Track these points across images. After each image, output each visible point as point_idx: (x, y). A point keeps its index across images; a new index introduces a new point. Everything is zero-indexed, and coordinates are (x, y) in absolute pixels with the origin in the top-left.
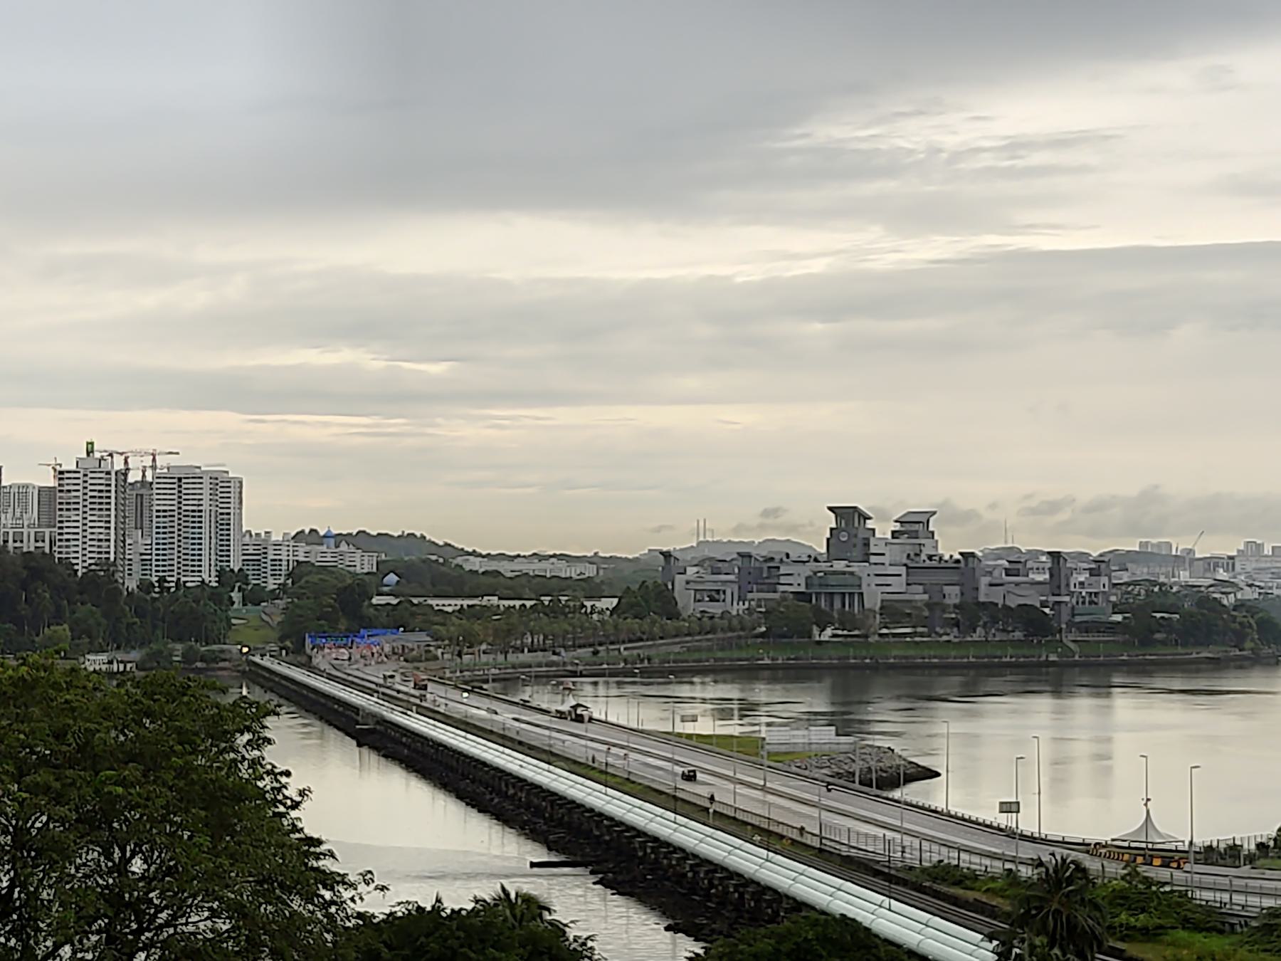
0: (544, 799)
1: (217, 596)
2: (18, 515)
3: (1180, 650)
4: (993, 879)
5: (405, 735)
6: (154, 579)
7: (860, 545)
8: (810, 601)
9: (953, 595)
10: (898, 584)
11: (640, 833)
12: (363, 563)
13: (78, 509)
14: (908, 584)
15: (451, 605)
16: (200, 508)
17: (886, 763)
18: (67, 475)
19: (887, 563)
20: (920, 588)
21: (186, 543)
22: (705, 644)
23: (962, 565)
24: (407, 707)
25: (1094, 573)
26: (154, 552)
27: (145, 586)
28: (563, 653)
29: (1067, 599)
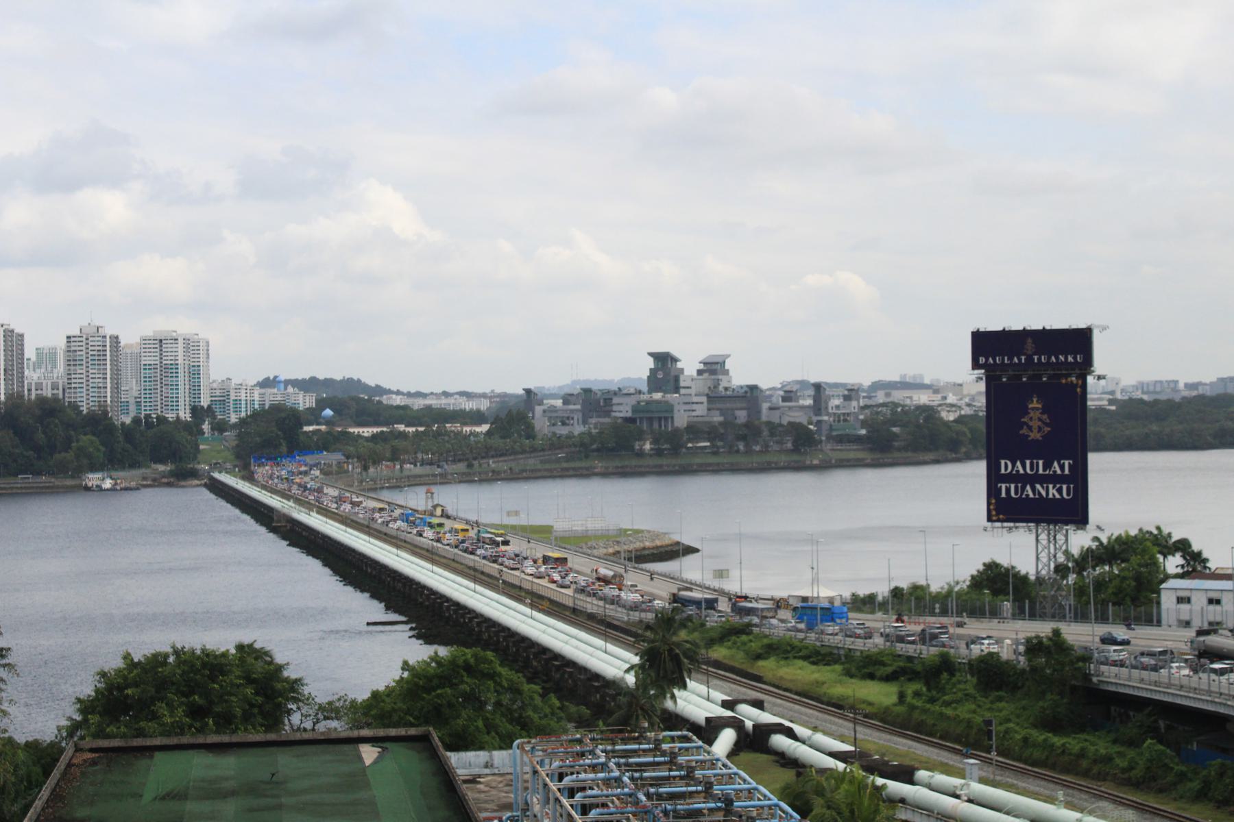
0: (389, 576)
1: (193, 428)
2: (49, 369)
3: (909, 454)
5: (304, 530)
6: (142, 416)
9: (742, 416)
10: (701, 410)
11: (448, 599)
12: (304, 401)
13: (82, 365)
14: (709, 409)
15: (367, 432)
16: (177, 362)
17: (658, 543)
18: (73, 339)
19: (693, 394)
24: (309, 506)
25: (847, 398)
27: (136, 421)
29: (826, 418)
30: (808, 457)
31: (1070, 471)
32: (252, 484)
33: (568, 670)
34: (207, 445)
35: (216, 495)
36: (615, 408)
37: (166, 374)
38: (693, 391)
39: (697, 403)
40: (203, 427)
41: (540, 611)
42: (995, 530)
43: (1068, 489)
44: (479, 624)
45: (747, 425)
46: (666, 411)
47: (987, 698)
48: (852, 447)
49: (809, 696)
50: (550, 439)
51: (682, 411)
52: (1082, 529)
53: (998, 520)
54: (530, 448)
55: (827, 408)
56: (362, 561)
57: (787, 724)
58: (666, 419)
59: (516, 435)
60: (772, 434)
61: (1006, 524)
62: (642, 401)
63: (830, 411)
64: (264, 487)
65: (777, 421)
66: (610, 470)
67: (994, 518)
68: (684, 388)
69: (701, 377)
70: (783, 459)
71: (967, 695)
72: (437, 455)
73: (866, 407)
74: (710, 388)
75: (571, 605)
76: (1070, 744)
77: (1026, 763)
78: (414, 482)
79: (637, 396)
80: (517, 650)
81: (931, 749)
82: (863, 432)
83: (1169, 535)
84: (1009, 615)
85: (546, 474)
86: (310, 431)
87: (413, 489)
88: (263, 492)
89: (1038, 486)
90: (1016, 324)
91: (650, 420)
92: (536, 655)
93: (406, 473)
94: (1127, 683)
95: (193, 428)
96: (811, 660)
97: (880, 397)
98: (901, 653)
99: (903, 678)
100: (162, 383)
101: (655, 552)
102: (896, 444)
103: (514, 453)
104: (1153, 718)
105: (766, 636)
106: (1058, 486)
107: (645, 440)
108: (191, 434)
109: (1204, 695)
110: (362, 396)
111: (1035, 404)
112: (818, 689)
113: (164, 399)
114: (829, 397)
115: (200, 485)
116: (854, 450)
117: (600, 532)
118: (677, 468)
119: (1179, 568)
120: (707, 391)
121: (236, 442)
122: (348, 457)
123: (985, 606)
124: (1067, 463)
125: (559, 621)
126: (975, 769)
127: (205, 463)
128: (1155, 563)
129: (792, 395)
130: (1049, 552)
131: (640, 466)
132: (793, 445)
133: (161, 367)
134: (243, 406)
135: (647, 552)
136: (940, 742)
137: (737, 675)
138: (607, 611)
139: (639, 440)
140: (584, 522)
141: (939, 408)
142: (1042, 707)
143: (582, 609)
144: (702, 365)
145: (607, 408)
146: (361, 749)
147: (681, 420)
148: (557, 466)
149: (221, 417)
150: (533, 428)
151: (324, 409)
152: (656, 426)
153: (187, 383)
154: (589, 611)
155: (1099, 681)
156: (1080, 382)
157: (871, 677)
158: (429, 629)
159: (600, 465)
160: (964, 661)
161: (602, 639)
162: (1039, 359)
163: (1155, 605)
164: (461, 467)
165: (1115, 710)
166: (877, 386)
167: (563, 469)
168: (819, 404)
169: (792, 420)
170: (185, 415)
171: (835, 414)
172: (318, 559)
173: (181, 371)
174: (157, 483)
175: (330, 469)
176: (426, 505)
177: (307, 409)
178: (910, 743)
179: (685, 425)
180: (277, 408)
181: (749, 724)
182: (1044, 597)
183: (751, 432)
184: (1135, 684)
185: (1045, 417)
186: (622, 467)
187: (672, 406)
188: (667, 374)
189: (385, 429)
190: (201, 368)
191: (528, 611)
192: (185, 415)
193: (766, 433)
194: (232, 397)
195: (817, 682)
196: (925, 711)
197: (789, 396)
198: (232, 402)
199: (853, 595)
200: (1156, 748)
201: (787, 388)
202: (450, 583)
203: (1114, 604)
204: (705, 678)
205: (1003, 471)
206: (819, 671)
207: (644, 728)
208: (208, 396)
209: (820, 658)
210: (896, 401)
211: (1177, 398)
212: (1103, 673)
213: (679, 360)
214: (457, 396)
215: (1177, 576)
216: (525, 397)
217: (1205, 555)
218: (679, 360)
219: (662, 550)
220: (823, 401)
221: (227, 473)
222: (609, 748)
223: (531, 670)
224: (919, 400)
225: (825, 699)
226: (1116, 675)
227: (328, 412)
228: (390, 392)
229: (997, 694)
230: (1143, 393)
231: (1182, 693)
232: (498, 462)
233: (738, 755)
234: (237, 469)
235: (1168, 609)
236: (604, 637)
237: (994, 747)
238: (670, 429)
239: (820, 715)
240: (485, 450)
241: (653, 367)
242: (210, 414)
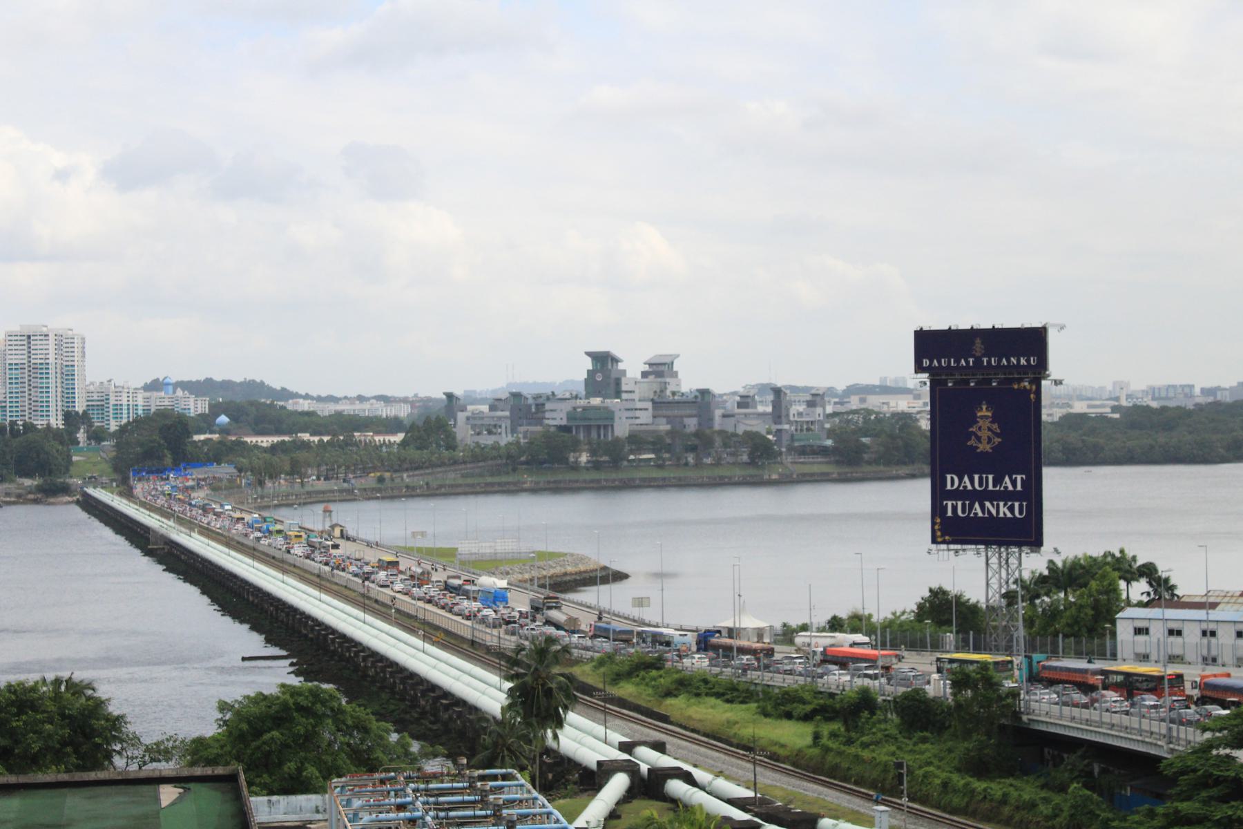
0: (271, 604)
1: (66, 437)
3: (882, 468)
5: (183, 553)
6: (7, 423)
7: (613, 386)
8: (571, 432)
9: (692, 424)
10: (645, 417)
12: (195, 406)
14: (654, 417)
15: (266, 441)
16: (47, 361)
17: (582, 568)
19: (637, 399)
21: (36, 392)
22: (477, 471)
23: (699, 400)
25: (811, 404)
26: (8, 400)
28: (353, 481)
29: (786, 427)
30: (766, 472)
31: (1022, 486)
32: (130, 501)
33: (457, 709)
34: (81, 456)
35: (89, 513)
36: (547, 415)
37: (35, 375)
38: (636, 396)
39: (641, 409)
40: (78, 435)
41: (433, 643)
42: (941, 553)
43: (1021, 507)
44: (365, 659)
45: (697, 434)
46: (607, 417)
47: (910, 739)
48: (816, 460)
49: (718, 738)
50: (472, 451)
51: (624, 419)
52: (1036, 552)
53: (944, 542)
54: (449, 460)
55: (788, 415)
56: (244, 589)
57: (686, 767)
58: (606, 427)
59: (434, 445)
60: (725, 445)
61: (952, 546)
62: (579, 407)
63: (792, 418)
64: (143, 505)
65: (730, 429)
66: (541, 485)
67: (939, 540)
68: (626, 392)
69: (645, 380)
70: (738, 473)
71: (886, 736)
72: (343, 468)
73: (835, 414)
74: (655, 392)
75: (469, 637)
76: (991, 789)
77: (944, 811)
78: (311, 499)
79: (574, 401)
80: (405, 688)
81: (842, 795)
82: (829, 443)
83: (1134, 559)
84: (952, 647)
85: (467, 489)
86: (200, 441)
87: (309, 507)
88: (142, 510)
89: (988, 504)
90: (963, 322)
91: (588, 429)
92: (424, 693)
93: (308, 488)
94: (1057, 722)
95: (66, 437)
96: (727, 697)
97: (854, 403)
98: (822, 690)
99: (819, 717)
100: (30, 385)
101: (578, 578)
102: (866, 456)
103: (433, 466)
104: (1086, 762)
105: (678, 671)
106: (1010, 503)
107: (581, 451)
108: (62, 443)
109: (1135, 734)
110: (263, 400)
111: (984, 412)
112: (728, 730)
113: (33, 404)
114: (791, 403)
115: (72, 502)
116: (820, 463)
117: (510, 555)
118: (617, 483)
119: (1145, 595)
120: (652, 396)
121: (114, 453)
122: (240, 471)
123: (926, 637)
124: (1019, 477)
125: (453, 655)
126: (885, 817)
127: (78, 476)
128: (1115, 590)
129: (749, 400)
130: (1001, 578)
131: (577, 481)
132: (749, 458)
133: (30, 366)
134: (125, 412)
135: (568, 578)
136: (854, 788)
137: (642, 714)
138: (502, 641)
139: (574, 451)
140: (493, 544)
141: (918, 416)
142: (967, 749)
143: (481, 641)
144: (647, 366)
145: (540, 415)
146: (161, 790)
147: (622, 429)
148: (481, 480)
149: (99, 424)
150: (454, 438)
151: (218, 416)
152: (594, 435)
153: (59, 385)
154: (488, 644)
155: (1029, 720)
156: (1034, 387)
157: (788, 716)
158: (312, 664)
159: (530, 479)
160: (889, 698)
161: (496, 674)
162: (989, 362)
163: (1108, 636)
165: (1049, 753)
166: (853, 390)
167: (487, 484)
169: (749, 429)
170: (57, 422)
171: (796, 422)
172: (196, 585)
173: (52, 371)
174: (21, 499)
175: (220, 484)
176: (324, 526)
177: (199, 415)
178: (821, 788)
179: (627, 435)
180: (163, 414)
181: (644, 768)
182: (995, 628)
183: (701, 442)
184: (1065, 723)
185: (995, 426)
186: (555, 482)
187: (613, 412)
188: (607, 376)
189: (287, 439)
190: (76, 368)
191: (419, 643)
192: (57, 422)
193: (718, 441)
194: (112, 401)
195: (728, 722)
196: (840, 753)
197: (745, 401)
198: (111, 407)
199: (785, 625)
200: (1081, 793)
202: (337, 612)
203: (1066, 636)
204: (602, 717)
205: (949, 487)
206: (732, 710)
207: (463, 765)
208: (84, 400)
209: (735, 694)
210: (870, 408)
211: (1190, 406)
212: (1034, 711)
213: (621, 361)
214: (373, 401)
215: (1140, 604)
216: (446, 403)
217: (1172, 582)
218: (621, 361)
219: (584, 575)
220: (783, 407)
221: (102, 488)
222: (422, 786)
223: (418, 710)
224: (897, 407)
225: (735, 741)
226: (1047, 713)
227: (223, 419)
228: (296, 396)
229: (921, 734)
230: (1154, 399)
231: (1113, 733)
232: (413, 476)
233: (631, 802)
234: (114, 484)
235: (1122, 641)
236: (498, 672)
237: (905, 792)
238: (610, 438)
239: (727, 758)
240: (398, 462)
241: (591, 368)
242: (86, 421)
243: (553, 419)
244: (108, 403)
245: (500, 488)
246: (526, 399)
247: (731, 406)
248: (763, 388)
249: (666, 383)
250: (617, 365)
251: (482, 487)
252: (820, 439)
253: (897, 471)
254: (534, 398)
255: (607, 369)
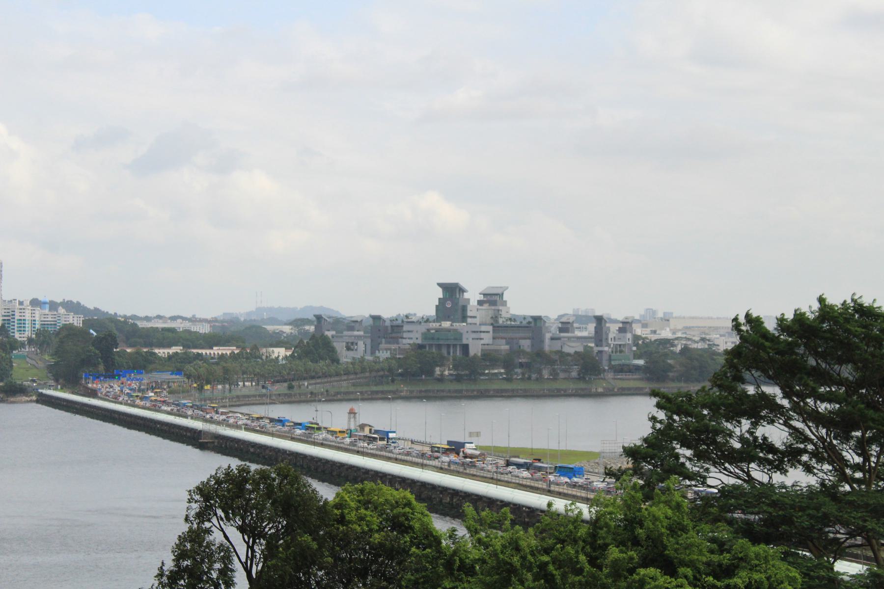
4: (212, 358)
7: (460, 311)
10: (487, 338)
14: (494, 338)
19: (478, 323)
20: (504, 341)
23: (532, 325)
29: (606, 349)
39: (484, 332)
55: (607, 339)
62: (432, 329)
66: (415, 394)
68: (471, 317)
70: (571, 386)
82: (641, 362)
102: (671, 374)
116: (634, 379)
129: (569, 326)
131: (443, 391)
144: (482, 296)
159: (405, 389)
164: (282, 388)
167: (373, 392)
168: (600, 335)
186: (426, 391)
187: (461, 334)
188: (455, 303)
194: (17, 317)
197: (565, 327)
198: (16, 322)
201: (564, 320)
243: (409, 338)
244: (14, 318)
245: (383, 396)
246: (384, 321)
247: (554, 329)
248: (583, 319)
249: (499, 310)
250: (463, 295)
251: (369, 395)
252: (629, 360)
253: (694, 387)
254: (391, 321)
255: (456, 297)
